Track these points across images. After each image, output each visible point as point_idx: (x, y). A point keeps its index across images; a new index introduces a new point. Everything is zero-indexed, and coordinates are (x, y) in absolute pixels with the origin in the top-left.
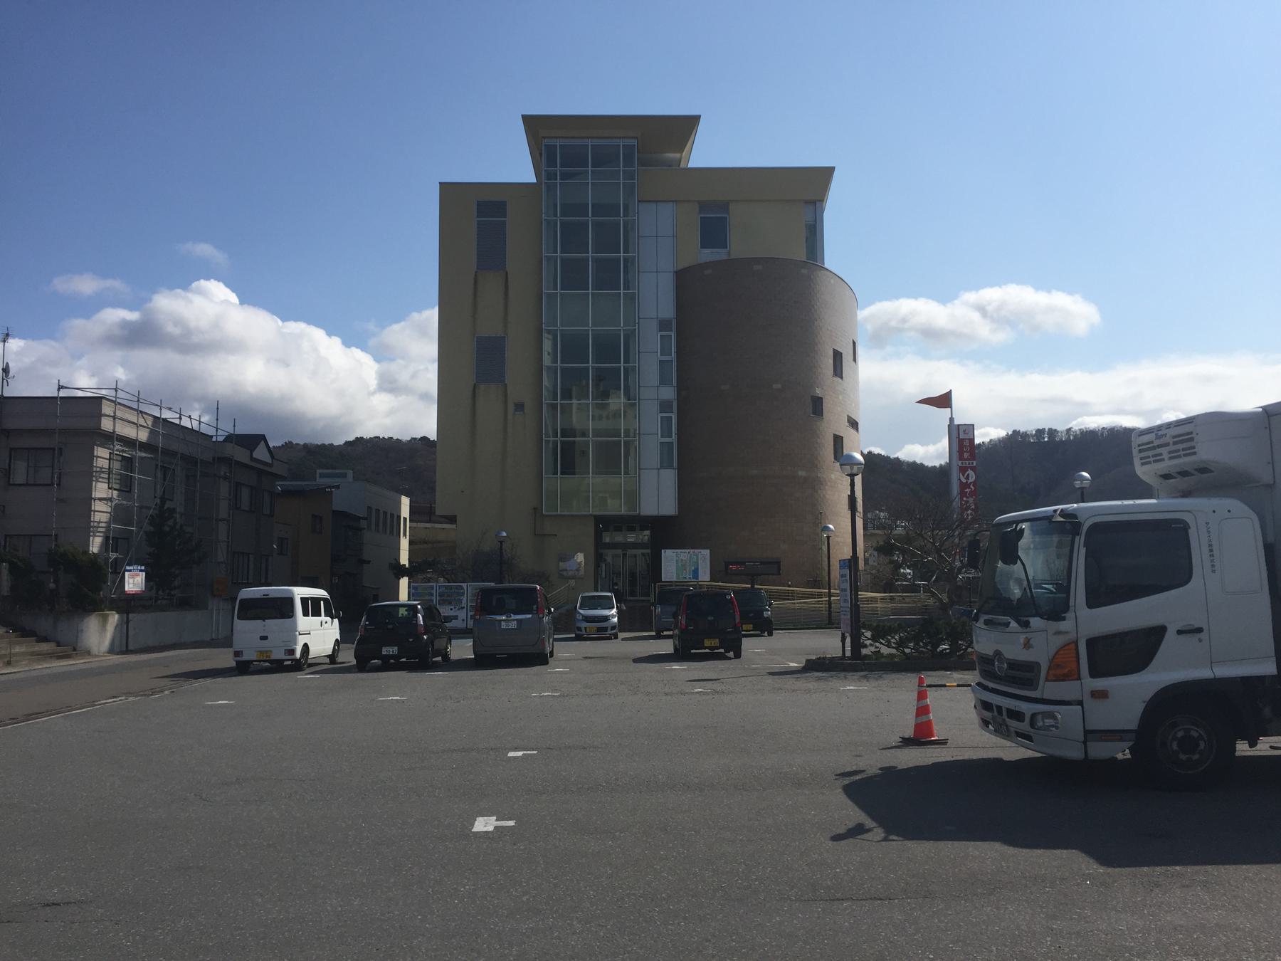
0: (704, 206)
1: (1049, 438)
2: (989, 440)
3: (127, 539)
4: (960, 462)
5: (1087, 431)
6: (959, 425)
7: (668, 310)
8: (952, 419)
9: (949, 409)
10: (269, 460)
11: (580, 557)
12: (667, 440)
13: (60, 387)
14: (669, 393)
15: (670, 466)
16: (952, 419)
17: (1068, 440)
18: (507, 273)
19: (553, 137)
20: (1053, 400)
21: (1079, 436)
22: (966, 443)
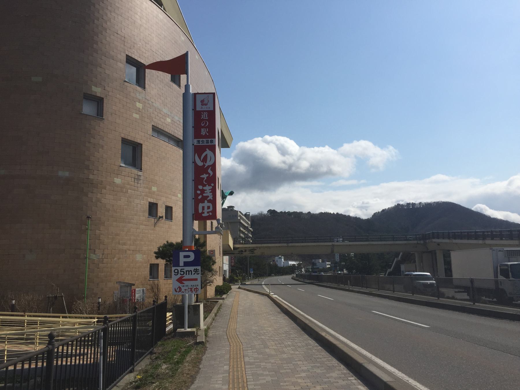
1: (412, 207)
4: (196, 141)
5: (427, 204)
6: (195, 94)
13: (506, 257)
17: (420, 207)
21: (425, 206)
22: (205, 116)
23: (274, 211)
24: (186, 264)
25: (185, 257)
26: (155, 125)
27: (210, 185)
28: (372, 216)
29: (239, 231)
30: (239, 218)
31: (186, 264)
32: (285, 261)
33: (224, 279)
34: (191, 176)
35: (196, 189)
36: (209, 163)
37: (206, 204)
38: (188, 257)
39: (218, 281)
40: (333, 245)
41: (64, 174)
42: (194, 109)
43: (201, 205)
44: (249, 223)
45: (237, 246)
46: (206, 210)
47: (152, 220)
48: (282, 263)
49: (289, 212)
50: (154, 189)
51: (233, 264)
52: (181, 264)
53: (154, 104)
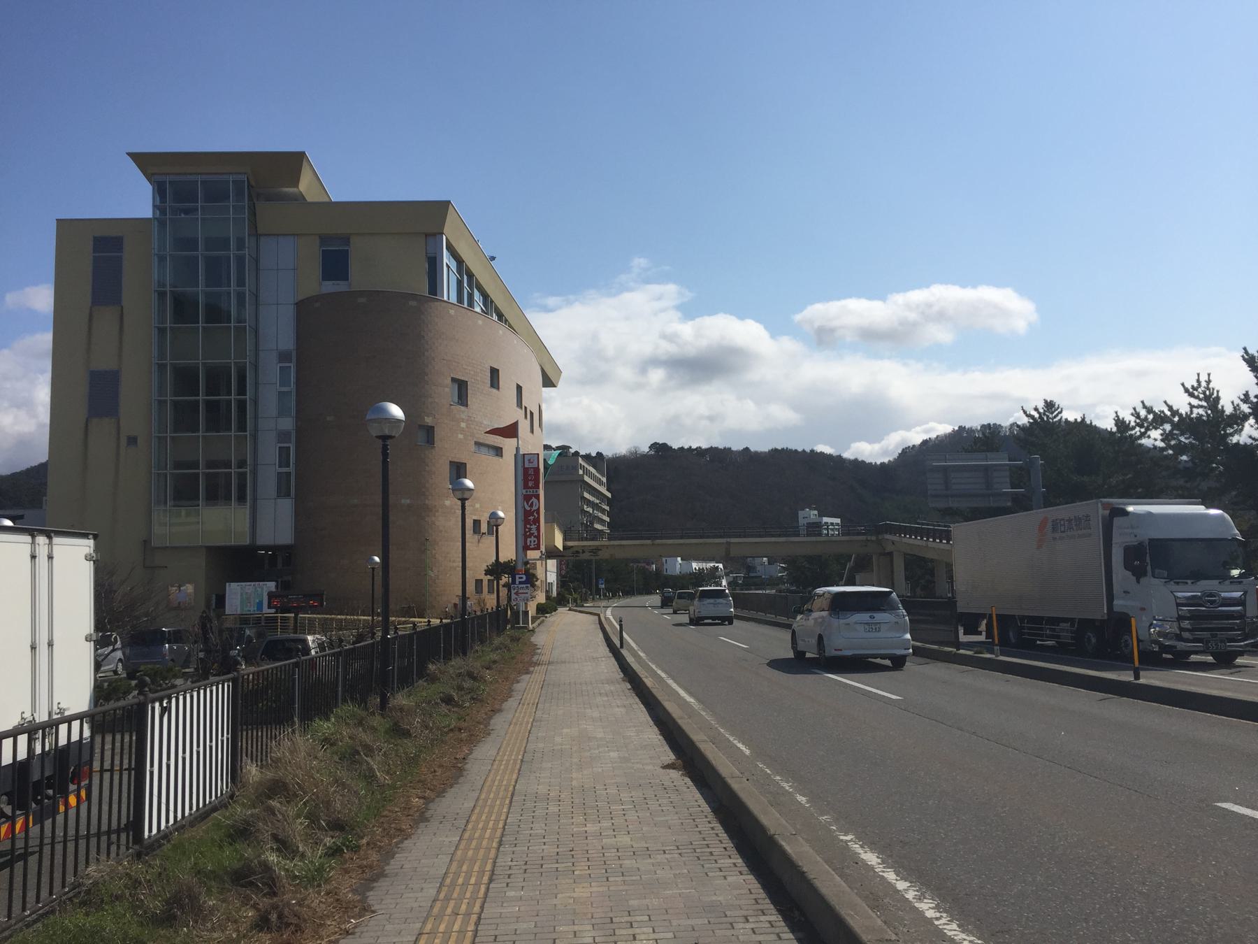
0: (324, 239)
2: (935, 436)
6: (524, 455)
8: (517, 449)
9: (516, 439)
11: (189, 588)
12: (285, 470)
14: (287, 424)
15: (288, 495)
16: (517, 449)
18: (122, 307)
20: (994, 397)
23: (665, 445)
24: (520, 583)
25: (520, 578)
27: (535, 525)
28: (898, 455)
29: (581, 498)
30: (581, 472)
31: (520, 583)
32: (684, 562)
33: (548, 598)
35: (525, 527)
36: (535, 508)
37: (533, 539)
38: (522, 578)
39: (541, 598)
40: (729, 543)
41: (406, 501)
43: (529, 540)
44: (604, 480)
45: (570, 544)
47: (476, 537)
48: (678, 566)
49: (700, 448)
50: (478, 506)
51: (563, 572)
52: (517, 583)
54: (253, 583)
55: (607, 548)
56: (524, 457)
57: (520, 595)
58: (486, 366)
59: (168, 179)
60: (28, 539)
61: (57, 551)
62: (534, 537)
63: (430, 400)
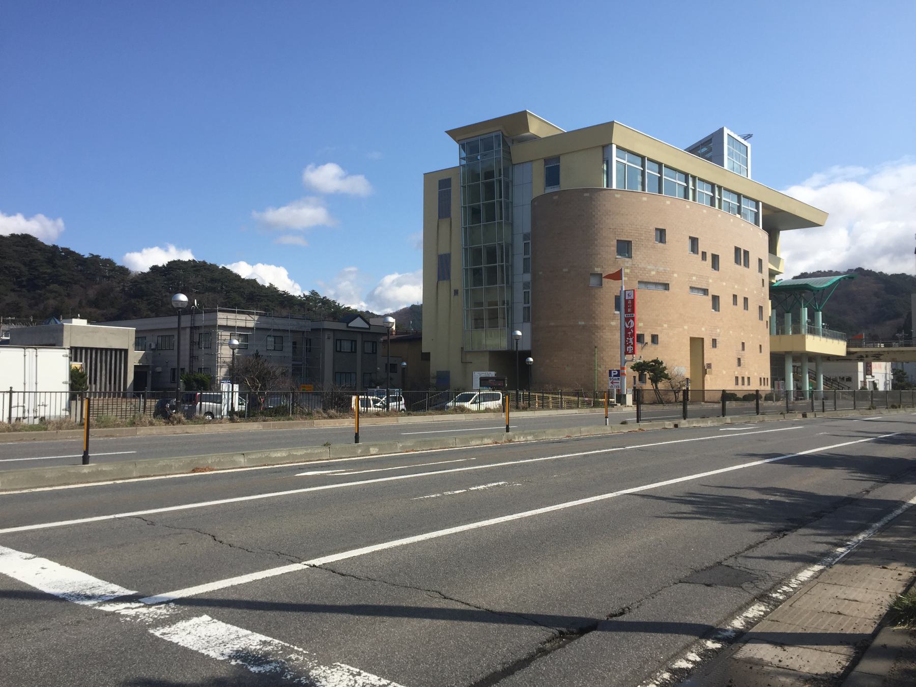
3: (364, 353)
7: (528, 229)
9: (75, 401)
10: (367, 326)
19: (476, 136)
22: (630, 302)
24: (615, 376)
26: (641, 280)
31: (615, 376)
34: (623, 333)
35: (626, 339)
37: (630, 347)
38: (615, 373)
41: (582, 323)
42: (625, 299)
43: (628, 347)
45: (853, 350)
46: (630, 350)
52: (612, 376)
53: (639, 266)
54: (484, 372)
55: (888, 353)
56: (625, 293)
57: (614, 384)
58: (651, 228)
59: (479, 138)
60: (23, 350)
61: (38, 353)
62: (631, 346)
63: (599, 256)
